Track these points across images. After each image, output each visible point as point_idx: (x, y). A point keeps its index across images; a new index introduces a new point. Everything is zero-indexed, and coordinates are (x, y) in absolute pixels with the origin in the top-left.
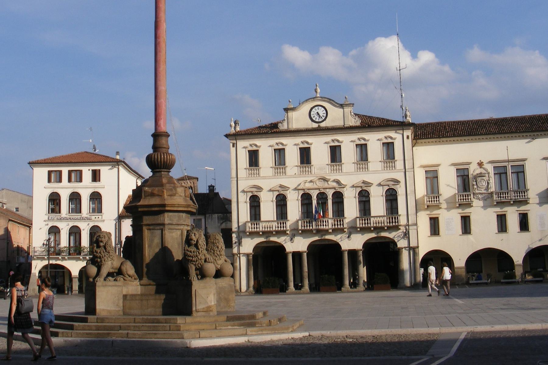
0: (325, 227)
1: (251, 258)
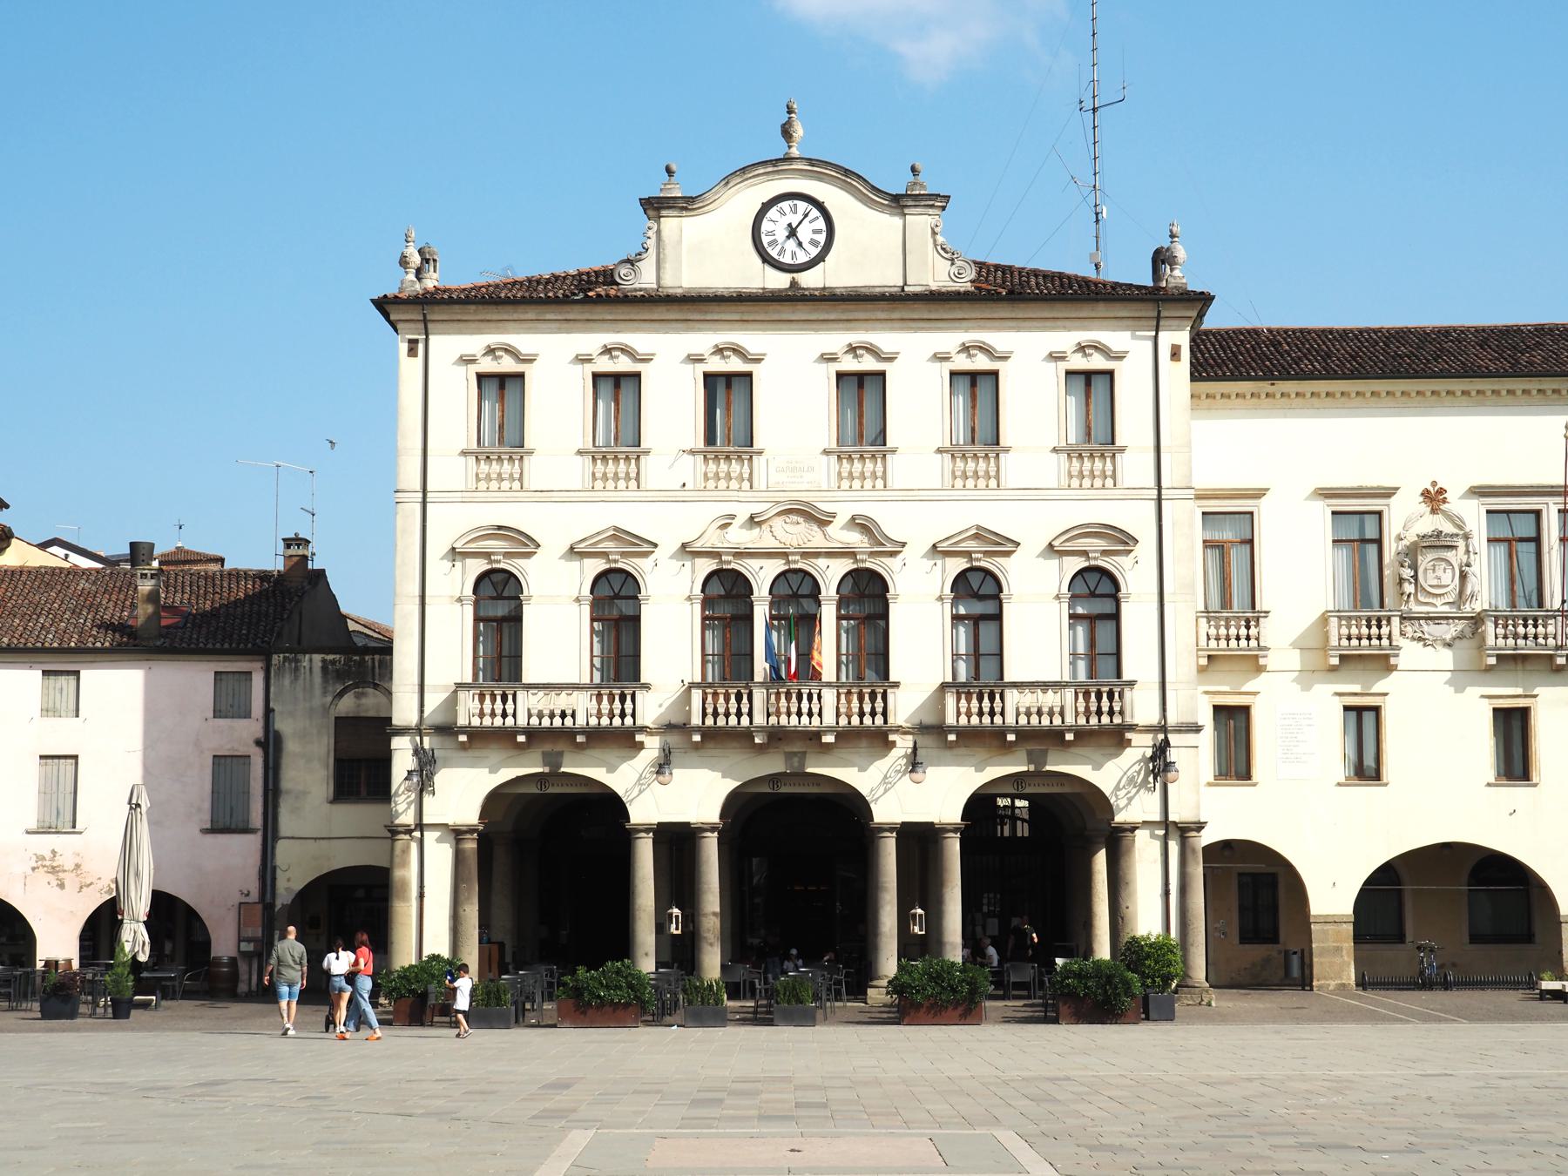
0: (805, 719)
1: (471, 845)
